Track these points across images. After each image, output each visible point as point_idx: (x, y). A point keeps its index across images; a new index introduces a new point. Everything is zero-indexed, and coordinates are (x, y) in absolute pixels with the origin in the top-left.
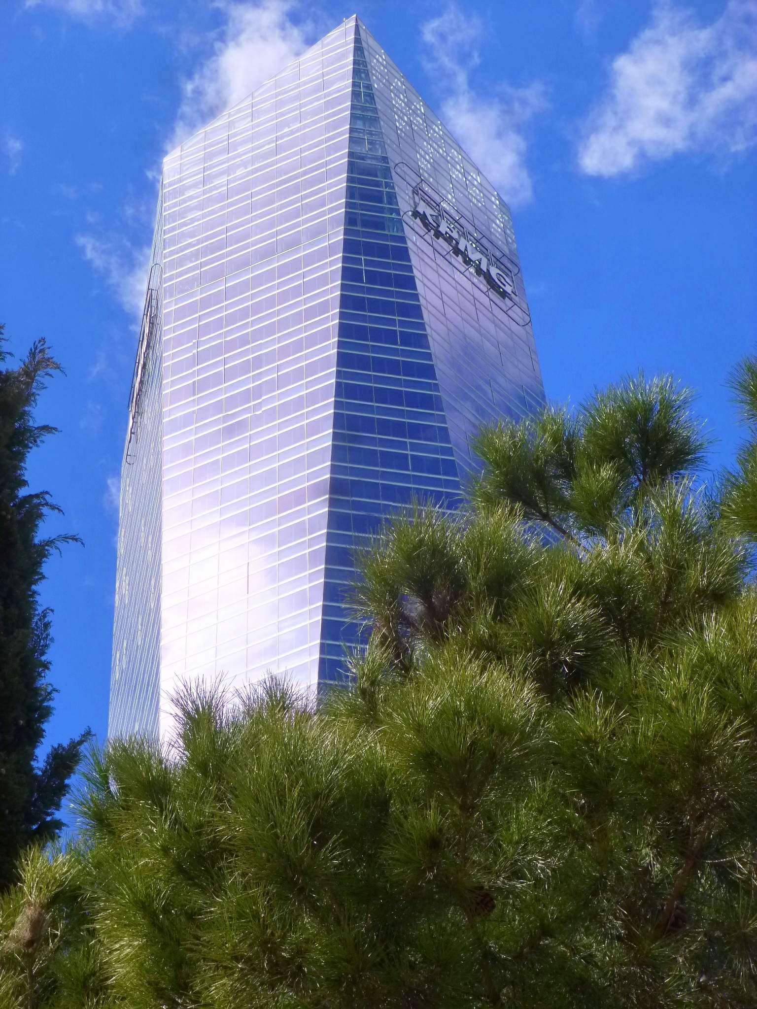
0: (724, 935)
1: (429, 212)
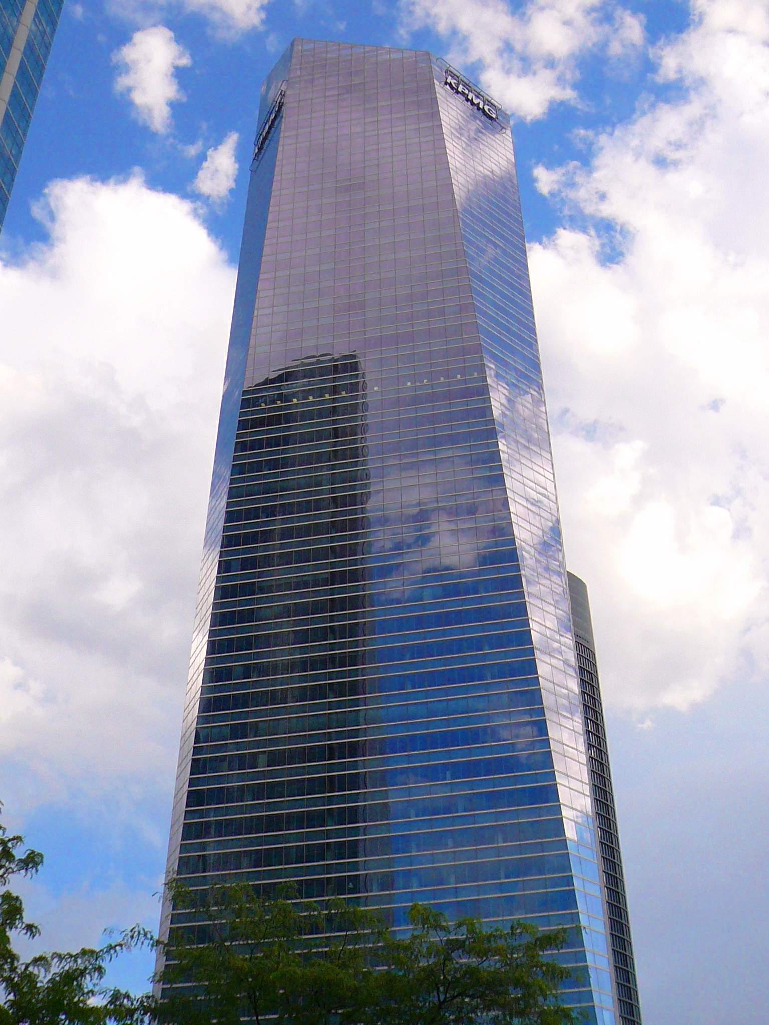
0: (400, 1019)
1: (453, 82)
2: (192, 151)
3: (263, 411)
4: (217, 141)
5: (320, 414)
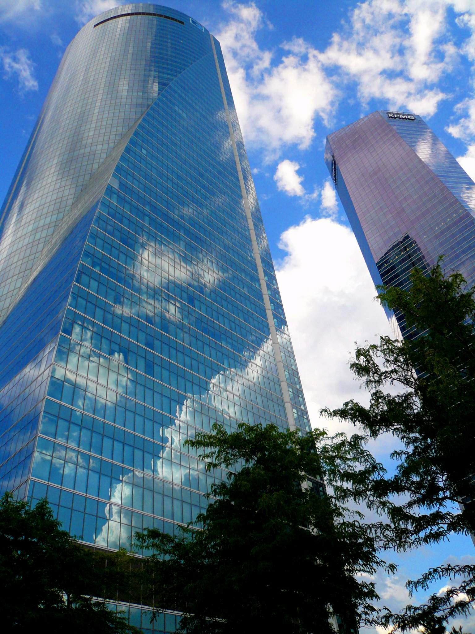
2: (315, 195)
3: (403, 255)
4: (322, 186)
5: (404, 260)
